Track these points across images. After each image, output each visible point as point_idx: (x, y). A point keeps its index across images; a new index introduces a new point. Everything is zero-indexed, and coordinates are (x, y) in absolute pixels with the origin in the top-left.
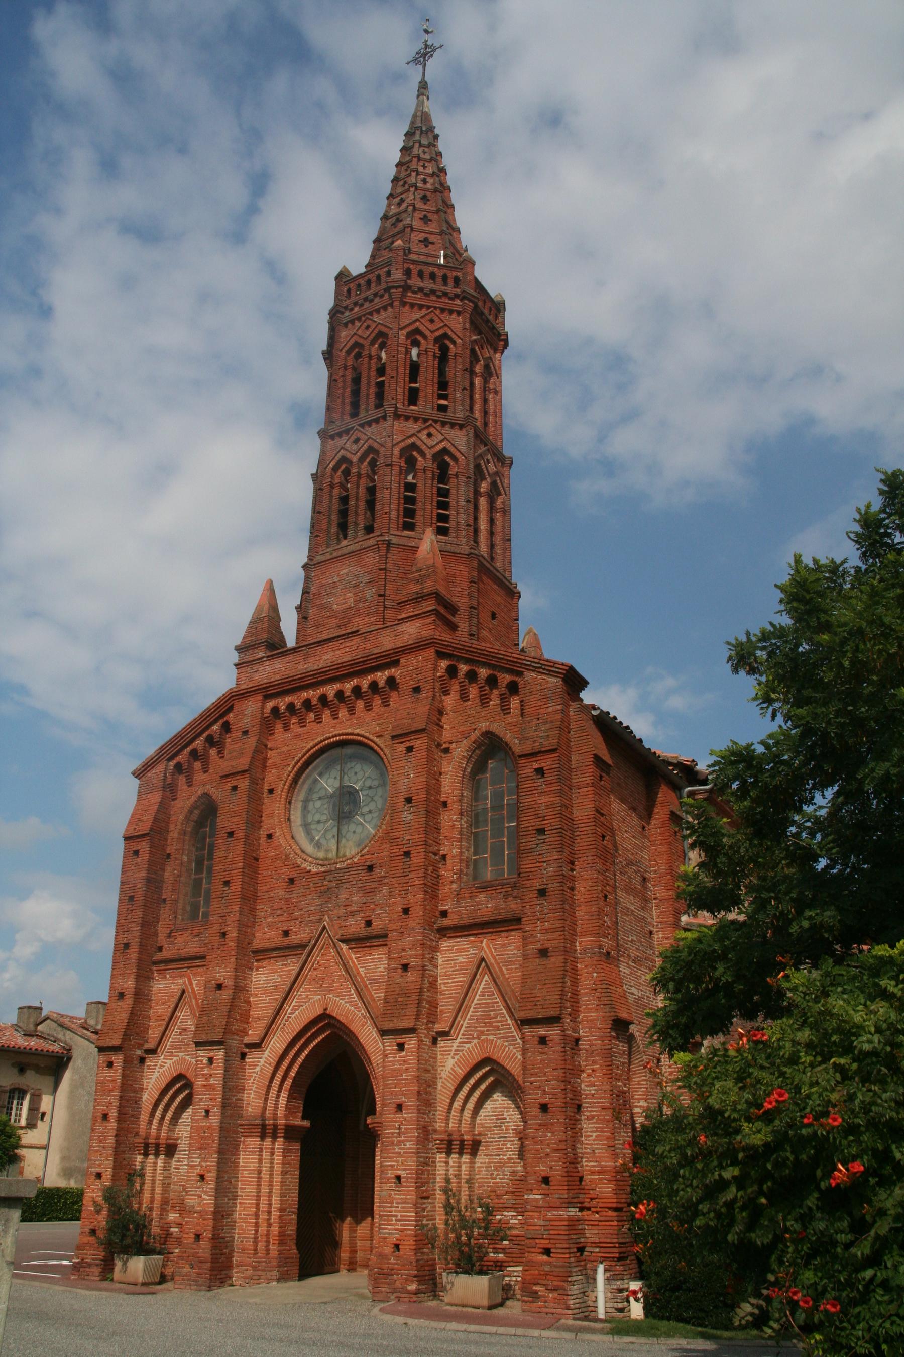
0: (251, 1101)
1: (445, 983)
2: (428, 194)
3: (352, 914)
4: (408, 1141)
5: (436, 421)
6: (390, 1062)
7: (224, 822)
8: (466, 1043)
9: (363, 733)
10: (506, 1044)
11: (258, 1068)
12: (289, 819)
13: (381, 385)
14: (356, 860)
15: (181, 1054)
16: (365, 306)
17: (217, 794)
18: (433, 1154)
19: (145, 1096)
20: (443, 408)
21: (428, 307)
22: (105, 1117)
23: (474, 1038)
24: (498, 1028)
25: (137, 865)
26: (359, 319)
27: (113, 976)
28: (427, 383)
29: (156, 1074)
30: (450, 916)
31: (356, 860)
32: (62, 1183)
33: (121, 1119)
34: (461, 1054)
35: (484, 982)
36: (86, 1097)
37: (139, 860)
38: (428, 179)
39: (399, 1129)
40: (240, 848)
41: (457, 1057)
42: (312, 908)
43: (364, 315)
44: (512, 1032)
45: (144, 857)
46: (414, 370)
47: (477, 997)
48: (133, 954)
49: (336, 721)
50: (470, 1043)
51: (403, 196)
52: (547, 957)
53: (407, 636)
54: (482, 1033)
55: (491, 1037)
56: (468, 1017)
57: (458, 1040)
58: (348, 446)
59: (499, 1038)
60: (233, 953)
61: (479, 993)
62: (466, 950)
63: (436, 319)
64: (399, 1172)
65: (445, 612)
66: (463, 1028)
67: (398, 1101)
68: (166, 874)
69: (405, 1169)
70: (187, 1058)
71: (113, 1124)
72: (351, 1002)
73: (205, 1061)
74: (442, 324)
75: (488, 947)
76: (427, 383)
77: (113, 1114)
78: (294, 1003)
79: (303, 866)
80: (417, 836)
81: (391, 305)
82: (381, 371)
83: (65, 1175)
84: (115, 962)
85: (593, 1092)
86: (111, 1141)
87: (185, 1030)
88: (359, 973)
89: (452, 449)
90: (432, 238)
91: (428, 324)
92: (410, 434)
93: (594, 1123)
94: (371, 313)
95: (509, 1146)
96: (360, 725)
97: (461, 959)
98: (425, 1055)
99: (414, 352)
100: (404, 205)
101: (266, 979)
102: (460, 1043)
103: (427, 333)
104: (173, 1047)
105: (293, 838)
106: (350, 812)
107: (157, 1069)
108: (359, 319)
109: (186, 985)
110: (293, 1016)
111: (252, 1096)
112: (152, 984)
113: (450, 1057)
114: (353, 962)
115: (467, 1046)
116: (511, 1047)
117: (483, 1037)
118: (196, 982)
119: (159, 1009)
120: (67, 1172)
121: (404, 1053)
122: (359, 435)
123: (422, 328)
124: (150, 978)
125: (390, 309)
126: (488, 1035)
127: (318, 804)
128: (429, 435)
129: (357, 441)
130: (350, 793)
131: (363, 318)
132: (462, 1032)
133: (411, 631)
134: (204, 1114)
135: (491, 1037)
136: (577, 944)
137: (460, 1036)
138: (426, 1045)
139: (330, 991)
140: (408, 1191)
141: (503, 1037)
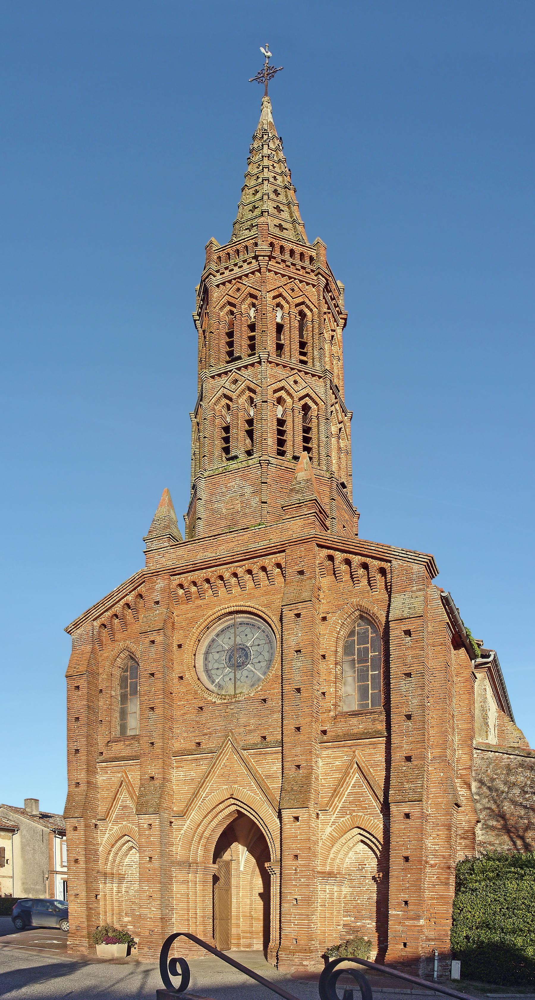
0: (178, 851)
1: (324, 779)
2: (278, 189)
3: (250, 731)
4: (302, 878)
5: (300, 371)
6: (288, 828)
7: (145, 667)
8: (342, 817)
9: (253, 605)
10: (372, 818)
11: (182, 832)
12: (195, 667)
13: (252, 338)
14: (252, 695)
15: (124, 823)
16: (234, 272)
17: (138, 649)
18: (317, 886)
19: (101, 849)
20: (304, 362)
21: (290, 278)
22: (76, 861)
23: (347, 814)
24: (366, 808)
25: (78, 696)
26: (230, 282)
27: (69, 771)
28: (291, 339)
29: (107, 836)
30: (329, 734)
31: (252, 695)
32: (23, 896)
33: (87, 862)
34: (337, 824)
35: (355, 778)
36: (32, 852)
37: (80, 693)
38: (278, 177)
39: (296, 870)
40: (160, 685)
41: (334, 826)
42: (218, 728)
43: (235, 279)
44: (377, 811)
45: (84, 690)
46: (280, 328)
47: (350, 788)
48: (82, 756)
49: (230, 596)
50: (344, 817)
51: (257, 188)
52: (411, 761)
53: (291, 532)
54: (354, 811)
55: (360, 814)
56: (343, 801)
57: (335, 815)
58: (227, 385)
59: (367, 815)
60: (160, 757)
61: (351, 785)
62: (342, 757)
63: (296, 288)
64: (296, 897)
65: (321, 515)
66: (339, 808)
67: (295, 853)
68: (101, 704)
69: (301, 895)
70: (129, 825)
71: (82, 865)
72: (251, 790)
73: (146, 826)
74: (301, 293)
75: (359, 755)
76: (291, 339)
77: (82, 859)
78: (207, 791)
79: (209, 698)
80: (306, 678)
81: (259, 271)
82: (252, 327)
83: (25, 892)
84: (69, 762)
85: (437, 849)
86: (83, 875)
87: (126, 807)
88: (257, 771)
89: (313, 395)
90: (285, 225)
91: (290, 292)
92: (280, 379)
93: (436, 869)
94: (240, 278)
95: (367, 882)
96: (250, 599)
97: (337, 763)
98: (313, 824)
99: (279, 314)
100: (259, 195)
101: (181, 776)
102: (336, 817)
103: (289, 299)
104: (117, 818)
105: (199, 679)
106: (243, 663)
107: (108, 832)
108: (230, 282)
109: (124, 778)
110: (207, 799)
111: (179, 849)
112: (97, 777)
113: (328, 826)
114: (252, 763)
115: (342, 819)
116: (376, 820)
117: (354, 814)
118: (134, 776)
119: (103, 796)
120: (26, 890)
121: (298, 823)
122: (237, 377)
123: (285, 294)
124: (95, 773)
125: (258, 274)
126: (358, 812)
127: (217, 656)
128: (296, 382)
129: (235, 382)
130: (243, 649)
131: (234, 282)
132: (338, 810)
133: (296, 527)
134: (148, 859)
135: (360, 814)
136: (429, 754)
137: (336, 813)
138: (313, 818)
139: (236, 783)
140: (303, 908)
141: (369, 814)
